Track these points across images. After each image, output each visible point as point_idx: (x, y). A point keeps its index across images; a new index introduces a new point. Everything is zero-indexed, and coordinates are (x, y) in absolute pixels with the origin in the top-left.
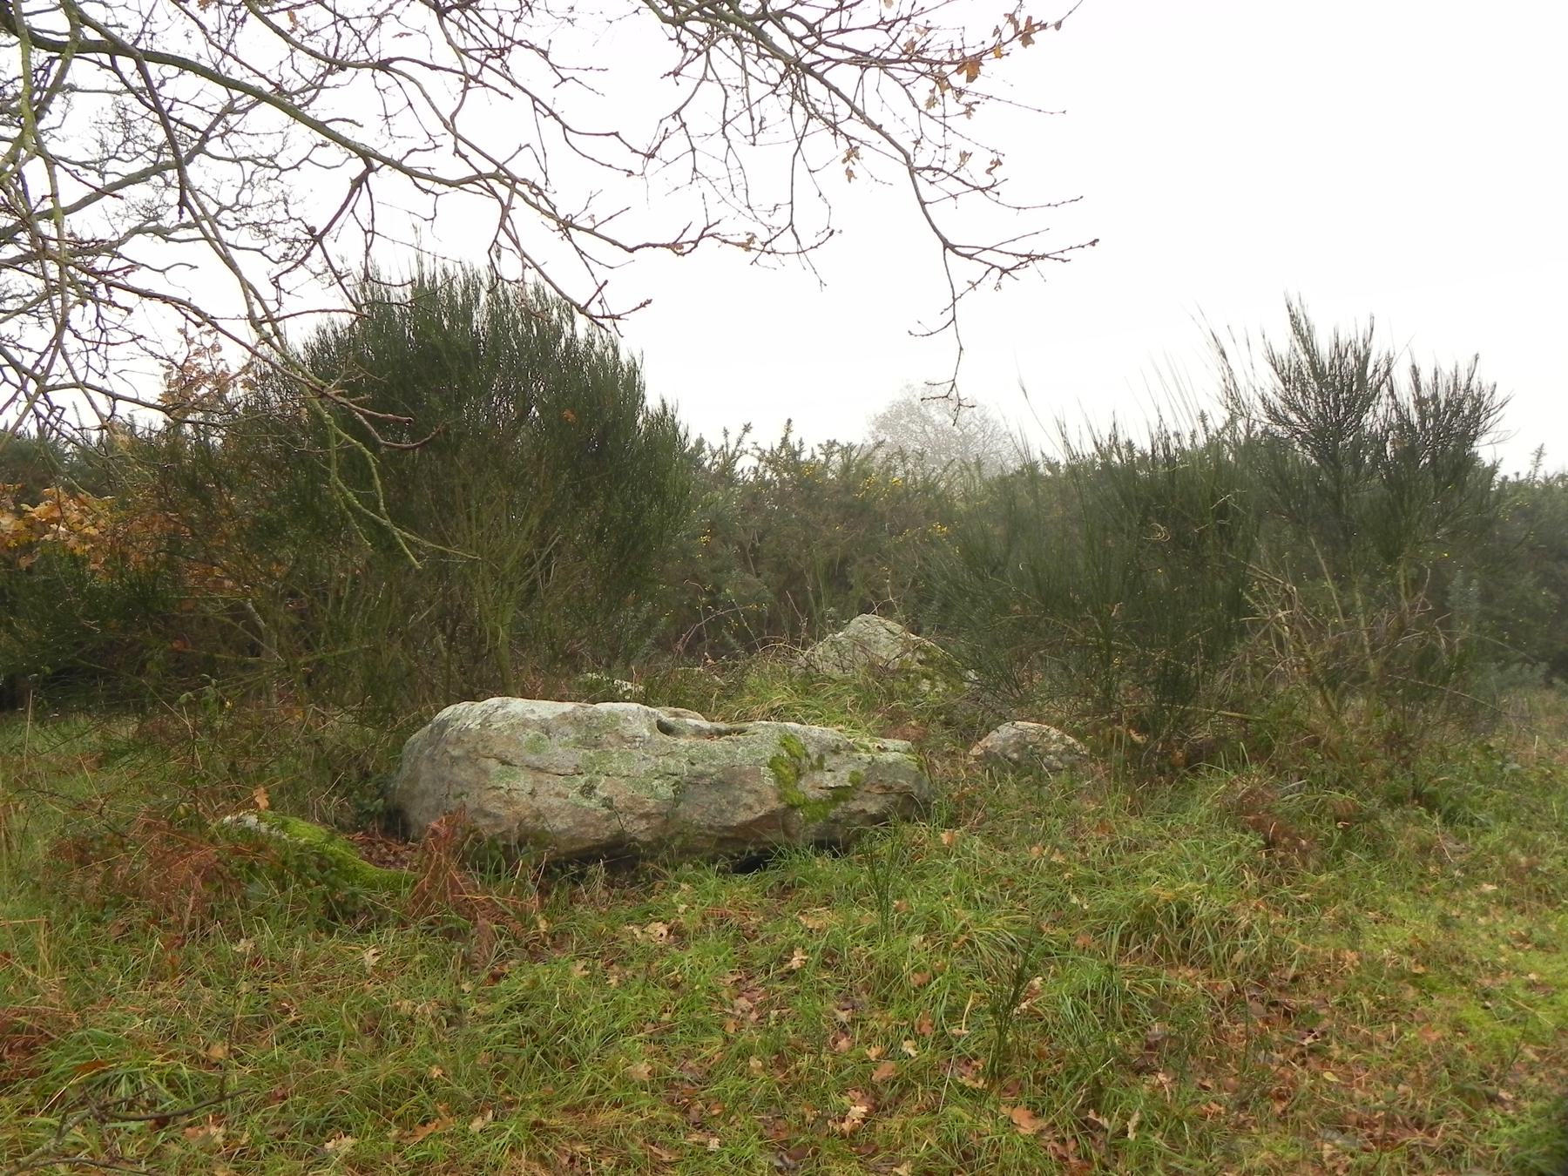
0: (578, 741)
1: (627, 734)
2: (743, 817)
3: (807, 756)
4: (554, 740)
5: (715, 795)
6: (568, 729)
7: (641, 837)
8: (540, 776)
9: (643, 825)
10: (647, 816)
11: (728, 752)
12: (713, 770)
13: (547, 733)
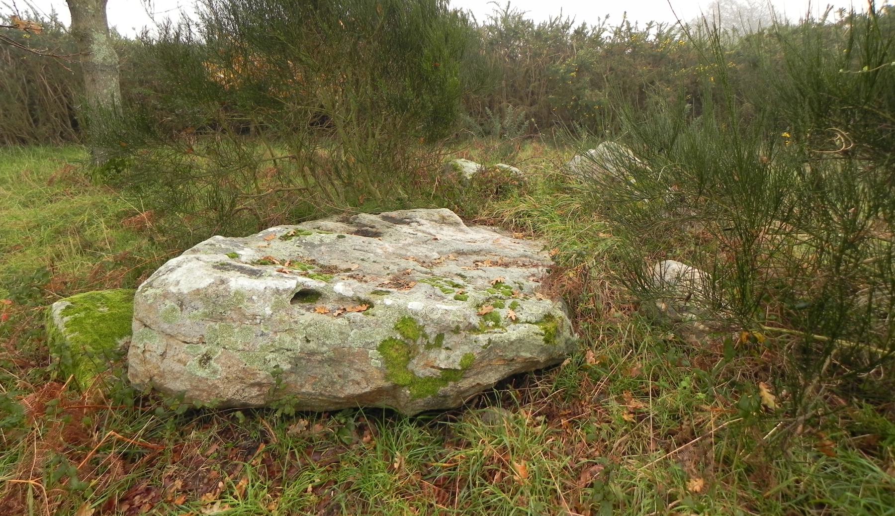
0: (205, 315)
1: (248, 313)
2: (351, 390)
3: (425, 336)
4: (186, 312)
5: (327, 368)
6: (199, 304)
7: (254, 402)
8: (171, 341)
9: (255, 392)
10: (260, 385)
11: (341, 333)
12: (325, 349)
13: (181, 306)
